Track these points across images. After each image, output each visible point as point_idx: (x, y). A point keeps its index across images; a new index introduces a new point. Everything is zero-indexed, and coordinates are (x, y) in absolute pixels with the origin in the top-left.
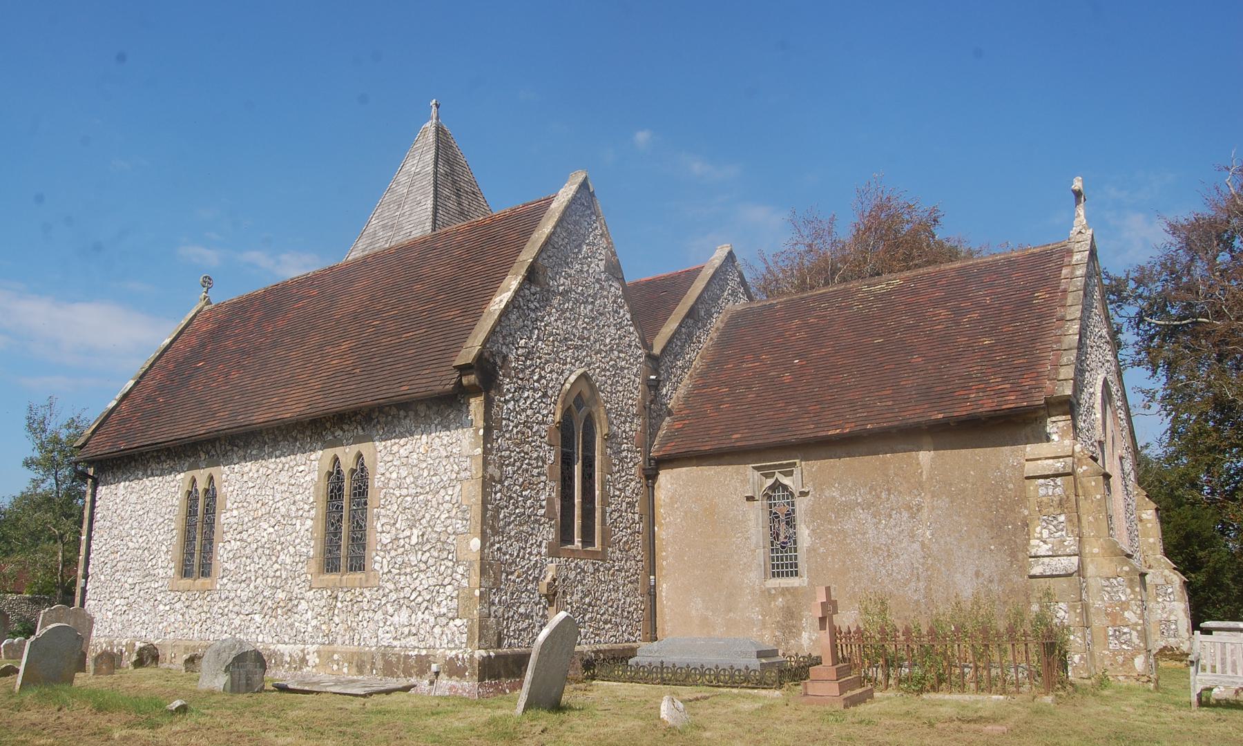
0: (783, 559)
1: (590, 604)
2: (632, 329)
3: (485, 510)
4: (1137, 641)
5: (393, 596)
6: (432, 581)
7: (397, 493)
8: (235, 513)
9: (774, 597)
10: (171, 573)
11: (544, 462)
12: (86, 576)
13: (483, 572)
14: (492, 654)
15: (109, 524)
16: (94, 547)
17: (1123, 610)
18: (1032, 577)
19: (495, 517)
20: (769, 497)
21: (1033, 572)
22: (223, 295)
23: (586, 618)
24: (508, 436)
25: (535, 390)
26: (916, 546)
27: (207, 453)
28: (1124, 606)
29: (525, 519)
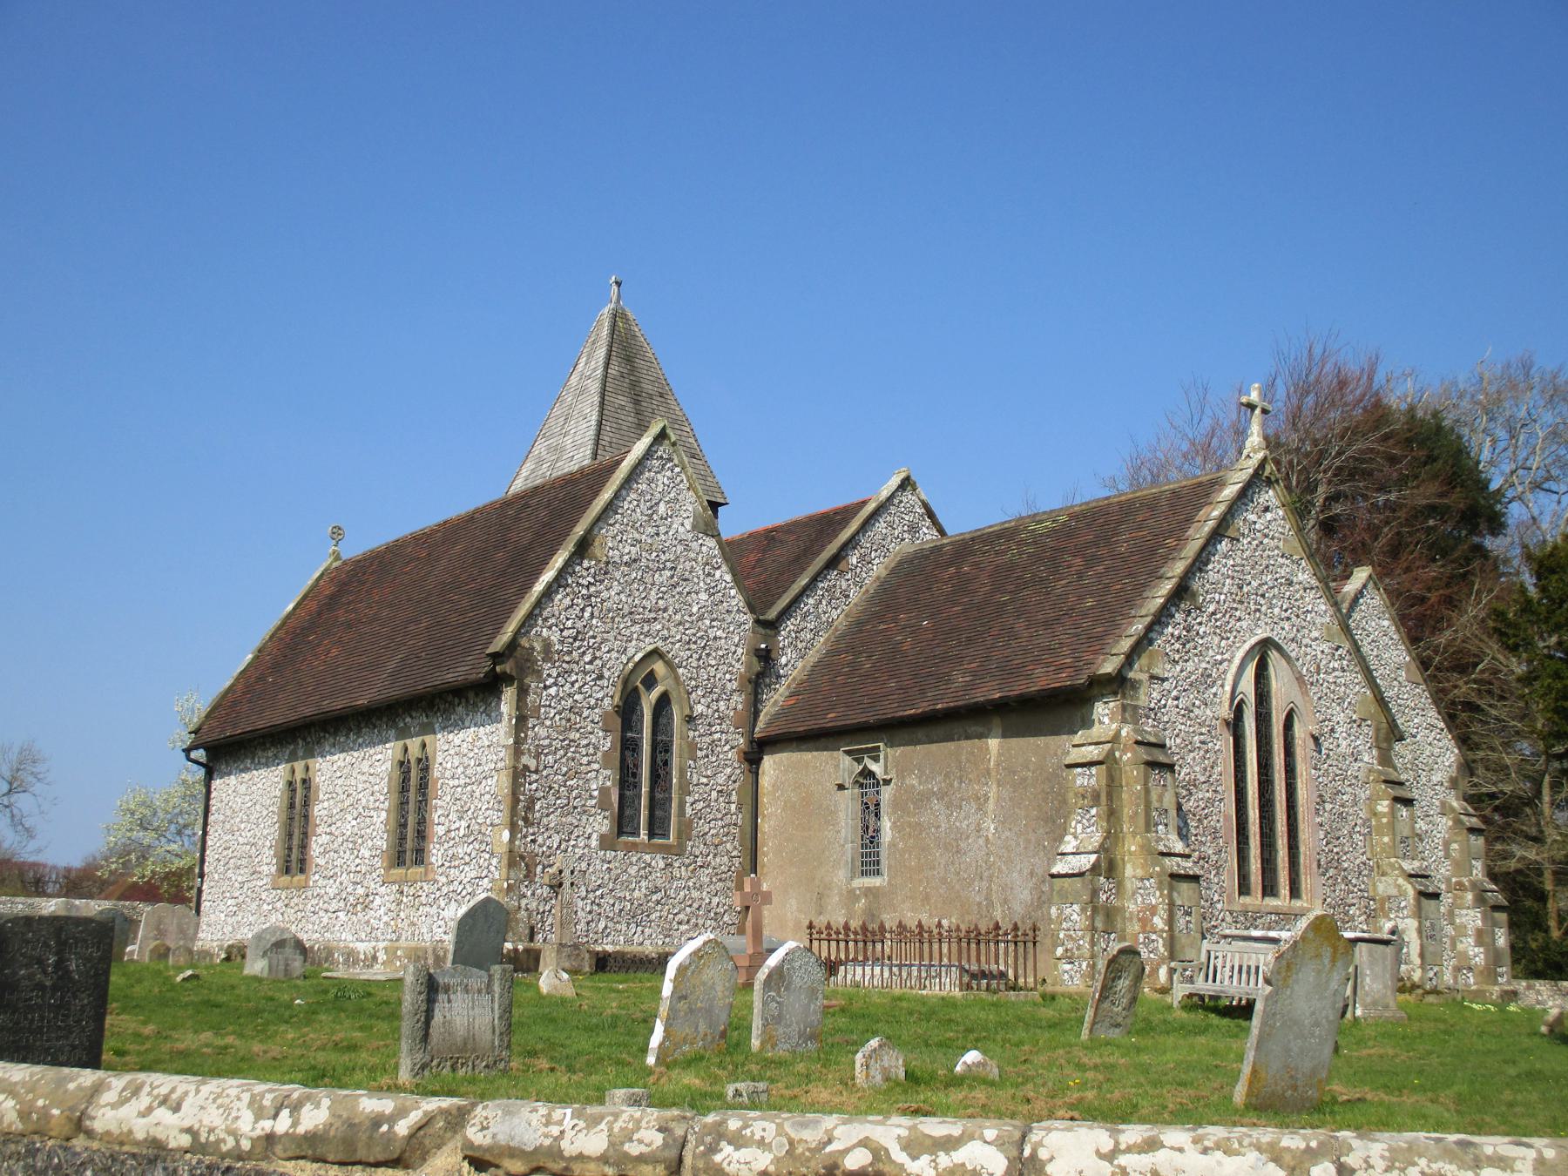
0: (869, 862)
1: (658, 902)
2: (733, 592)
3: (515, 801)
4: (1162, 949)
5: (445, 890)
6: (474, 874)
7: (451, 783)
8: (326, 804)
9: (857, 899)
10: (273, 869)
11: (596, 748)
12: (202, 875)
13: (512, 864)
14: (520, 947)
15: (222, 818)
16: (209, 843)
17: (1153, 914)
18: (1053, 876)
19: (530, 808)
20: (861, 786)
21: (1054, 871)
22: (355, 547)
23: (653, 917)
24: (548, 723)
25: (585, 673)
26: (981, 841)
27: (304, 739)
28: (1153, 910)
29: (568, 809)
